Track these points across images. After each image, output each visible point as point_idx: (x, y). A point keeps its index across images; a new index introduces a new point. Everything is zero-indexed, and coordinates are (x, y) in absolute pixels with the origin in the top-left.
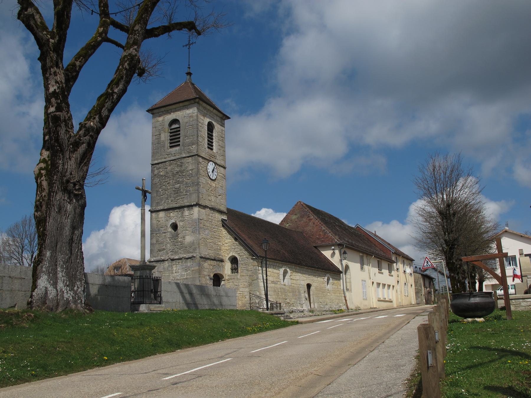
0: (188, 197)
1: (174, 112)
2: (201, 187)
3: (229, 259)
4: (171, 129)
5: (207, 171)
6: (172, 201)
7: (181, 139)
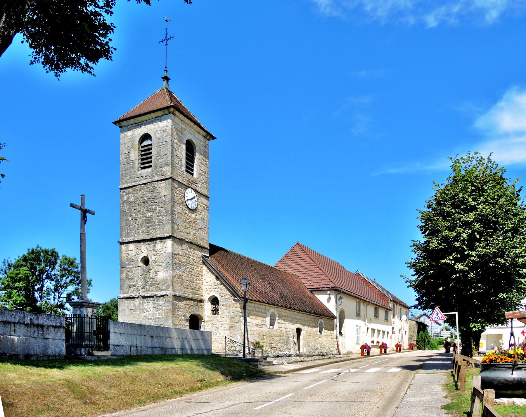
0: (161, 228)
1: (145, 125)
2: (176, 217)
3: (209, 299)
4: (142, 147)
5: (185, 199)
6: (143, 232)
7: (153, 159)
